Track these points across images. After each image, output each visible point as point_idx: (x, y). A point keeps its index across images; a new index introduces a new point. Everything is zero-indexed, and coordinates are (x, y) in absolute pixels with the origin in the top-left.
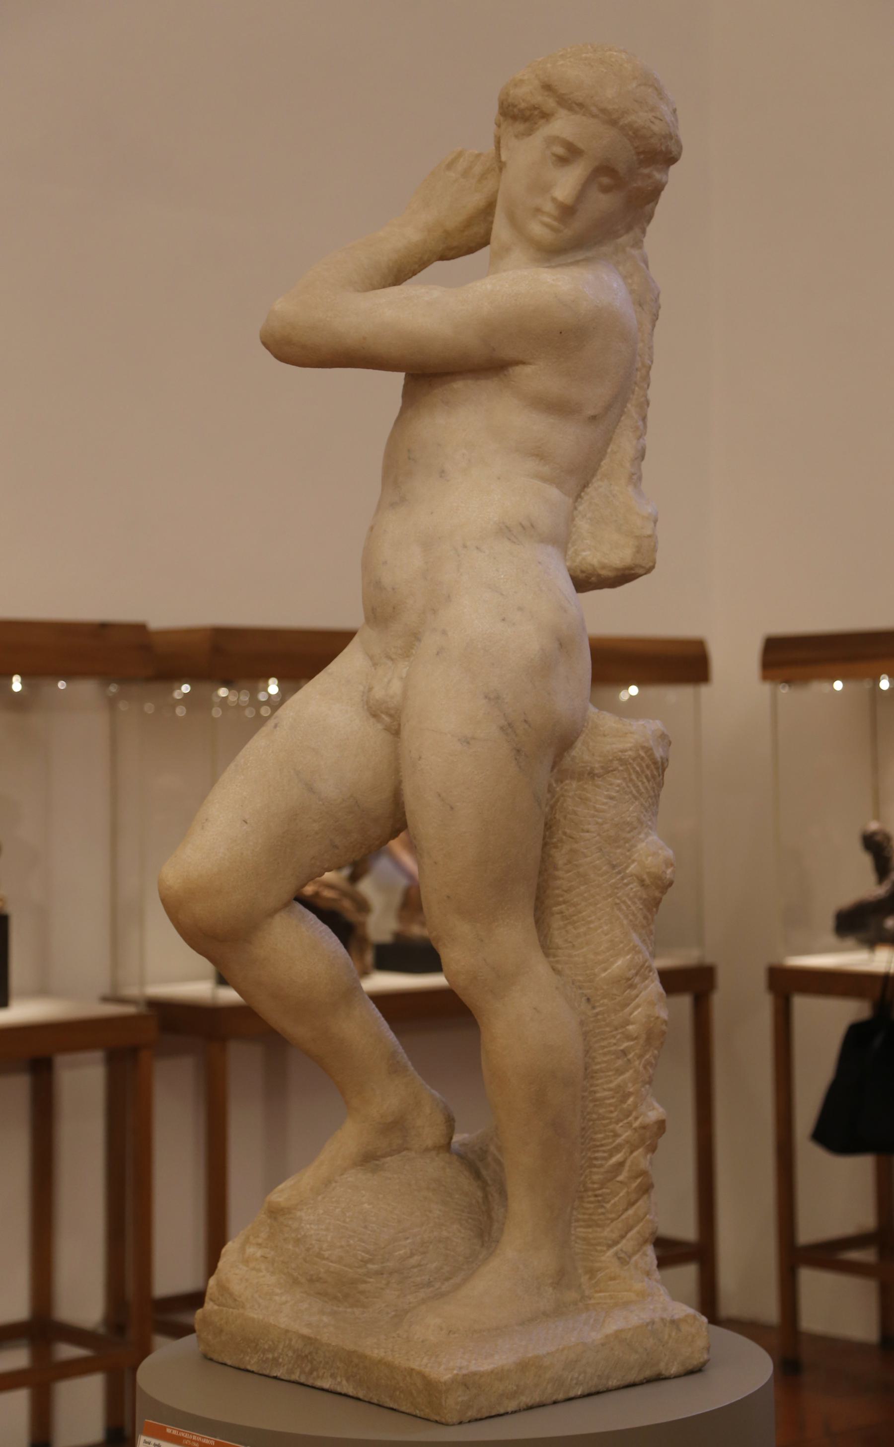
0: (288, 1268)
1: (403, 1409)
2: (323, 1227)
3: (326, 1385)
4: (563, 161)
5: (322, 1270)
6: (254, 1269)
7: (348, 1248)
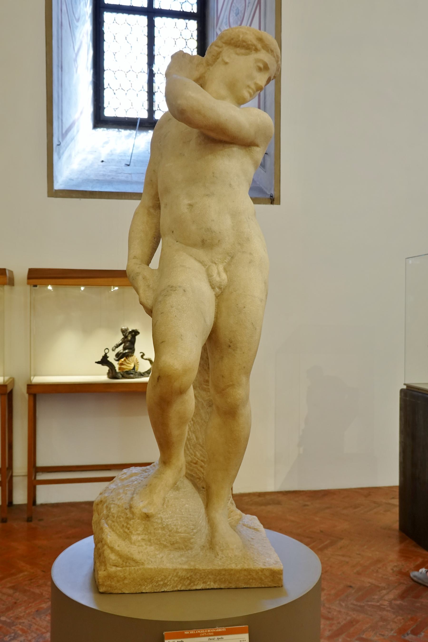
0: (160, 541)
1: (253, 586)
2: (175, 519)
4: (260, 69)
5: (178, 538)
6: (139, 546)
7: (187, 526)
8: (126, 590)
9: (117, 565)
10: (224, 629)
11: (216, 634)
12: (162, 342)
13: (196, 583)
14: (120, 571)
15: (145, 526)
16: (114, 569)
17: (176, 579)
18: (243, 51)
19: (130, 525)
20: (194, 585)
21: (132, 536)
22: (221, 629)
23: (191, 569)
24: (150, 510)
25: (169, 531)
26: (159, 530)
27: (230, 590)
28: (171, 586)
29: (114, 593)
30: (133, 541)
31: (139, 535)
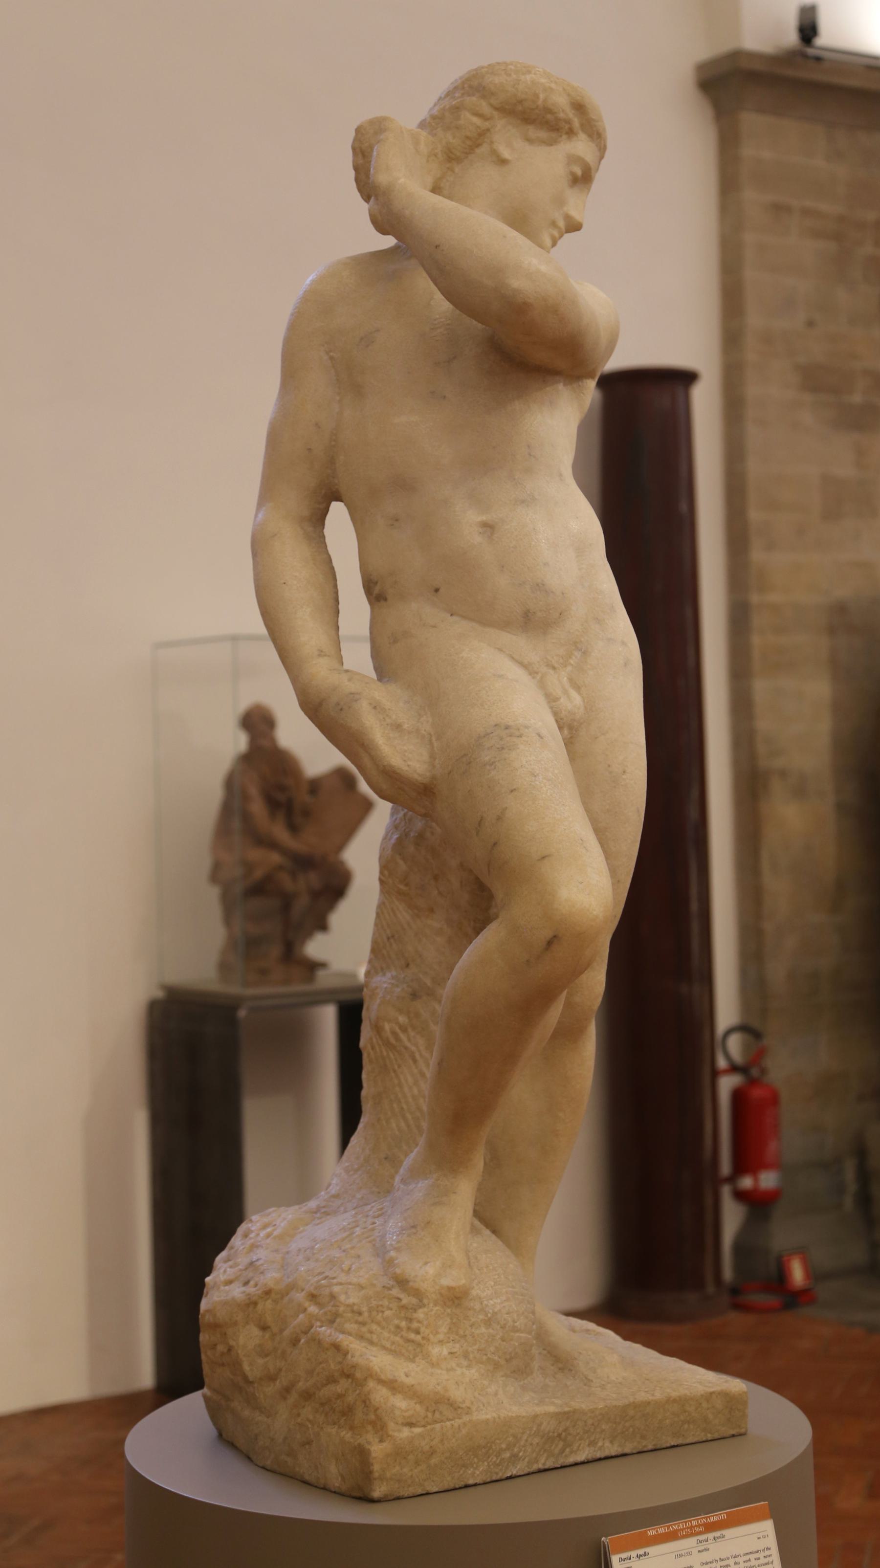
0: (486, 1355)
3: (581, 1457)
8: (432, 1484)
9: (414, 1421)
10: (722, 1515)
11: (710, 1528)
12: (543, 858)
13: (575, 1448)
14: (421, 1436)
15: (451, 1319)
16: (406, 1433)
17: (536, 1440)
18: (543, 134)
19: (419, 1322)
20: (571, 1452)
21: (430, 1348)
22: (717, 1515)
23: (565, 1413)
24: (453, 1279)
25: (501, 1327)
26: (480, 1326)
27: (644, 1454)
28: (527, 1460)
29: (406, 1495)
30: (434, 1360)
31: (442, 1345)
